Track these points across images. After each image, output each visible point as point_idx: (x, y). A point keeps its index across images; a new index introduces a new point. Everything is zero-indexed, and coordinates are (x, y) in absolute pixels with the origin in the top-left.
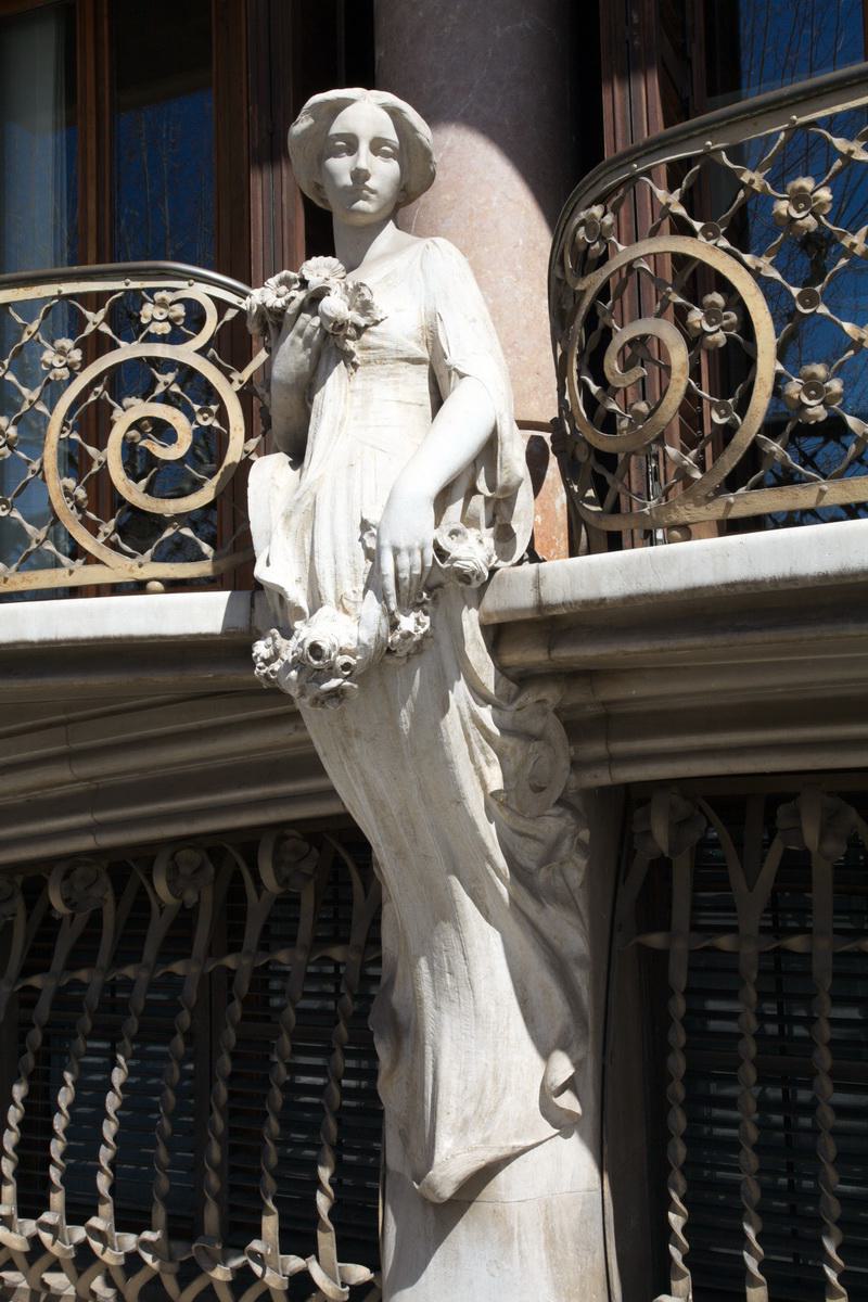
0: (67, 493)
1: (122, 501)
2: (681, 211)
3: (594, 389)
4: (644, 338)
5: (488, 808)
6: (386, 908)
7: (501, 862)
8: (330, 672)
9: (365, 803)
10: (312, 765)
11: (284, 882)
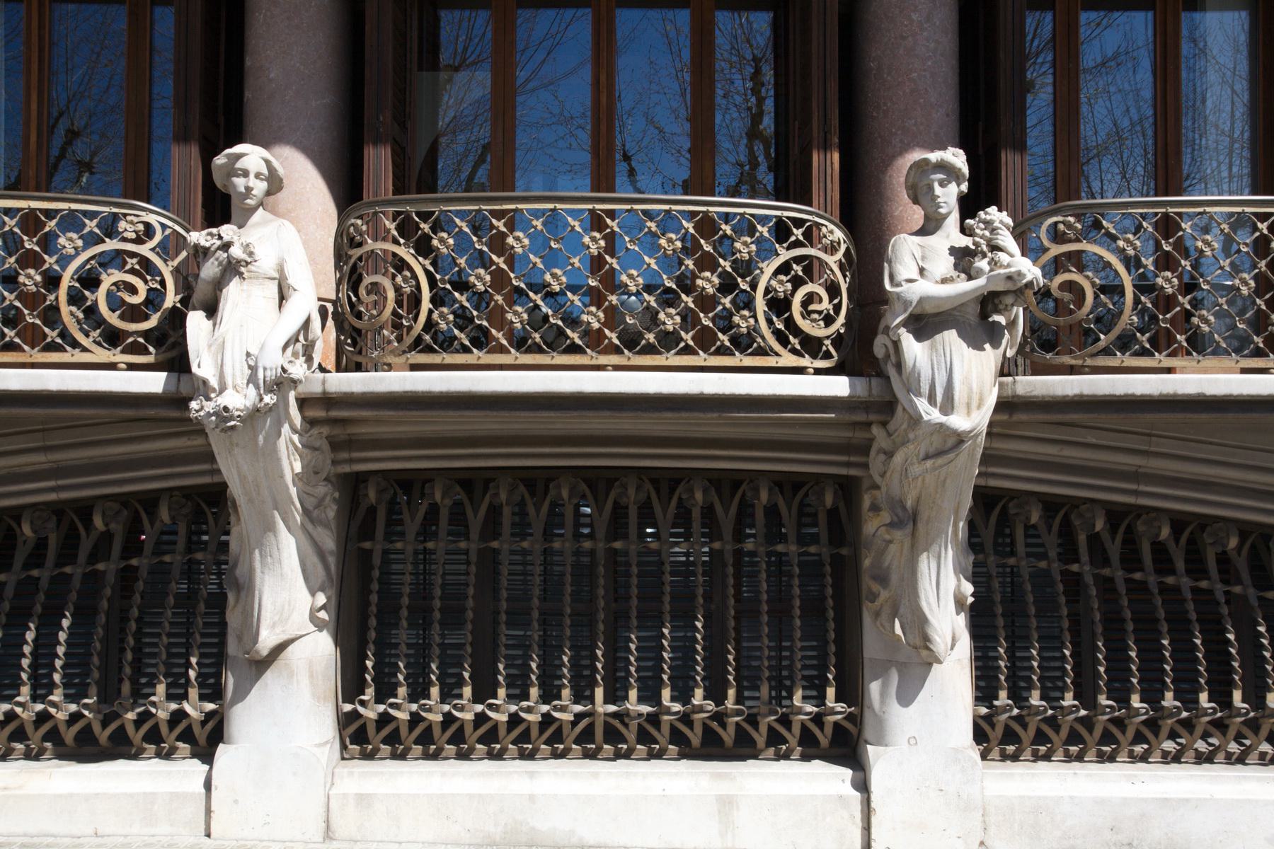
0: (72, 314)
1: (104, 321)
2: (395, 233)
3: (354, 299)
4: (376, 284)
5: (293, 480)
7: (298, 505)
8: (232, 418)
9: (236, 476)
10: (210, 457)
11: (173, 518)
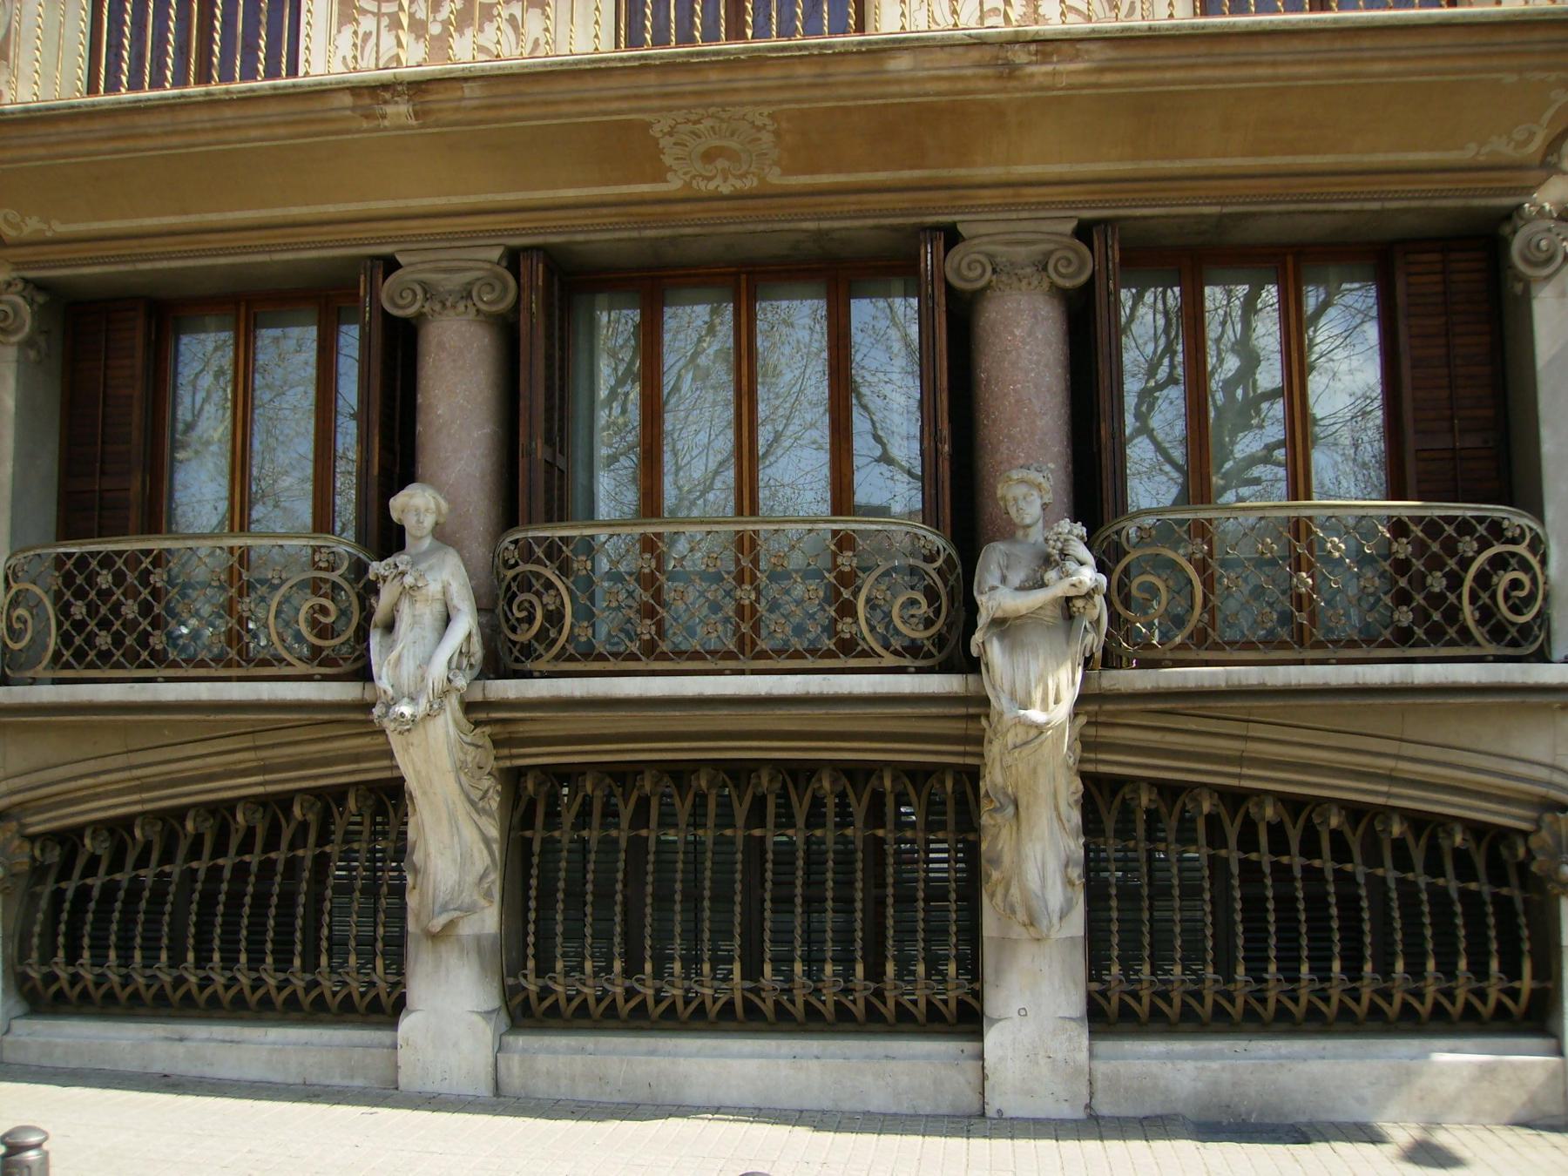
6: (412, 821)
9: (411, 771)
10: (390, 755)
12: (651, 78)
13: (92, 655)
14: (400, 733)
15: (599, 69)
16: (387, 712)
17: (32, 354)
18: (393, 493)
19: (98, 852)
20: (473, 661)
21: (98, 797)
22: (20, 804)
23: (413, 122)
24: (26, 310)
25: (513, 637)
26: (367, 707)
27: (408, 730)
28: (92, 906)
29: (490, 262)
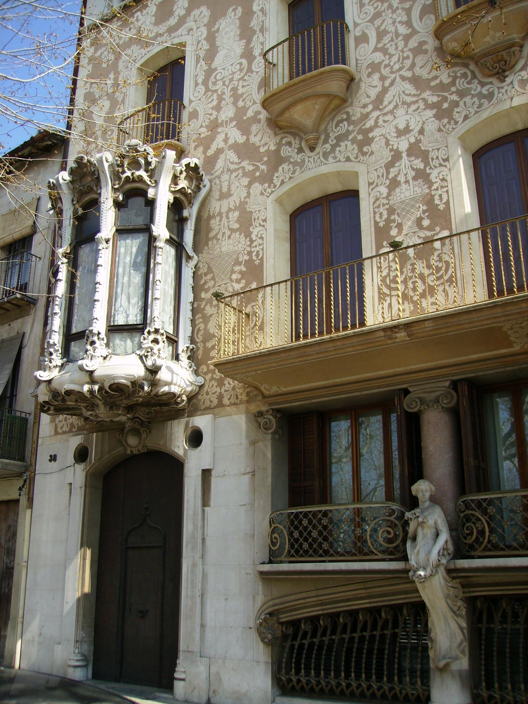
6: (429, 619)
10: (417, 591)
12: (499, 310)
13: (301, 552)
14: (420, 583)
15: (477, 309)
16: (415, 574)
17: (277, 436)
18: (412, 484)
19: (307, 630)
20: (449, 552)
21: (306, 607)
22: (277, 610)
23: (407, 339)
24: (274, 420)
25: (465, 541)
26: (407, 571)
27: (424, 582)
28: (305, 651)
29: (446, 387)
